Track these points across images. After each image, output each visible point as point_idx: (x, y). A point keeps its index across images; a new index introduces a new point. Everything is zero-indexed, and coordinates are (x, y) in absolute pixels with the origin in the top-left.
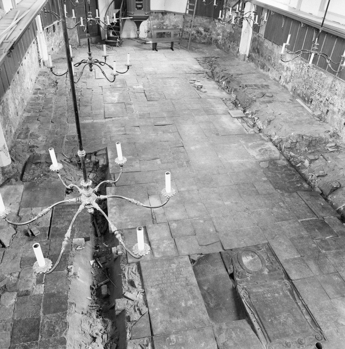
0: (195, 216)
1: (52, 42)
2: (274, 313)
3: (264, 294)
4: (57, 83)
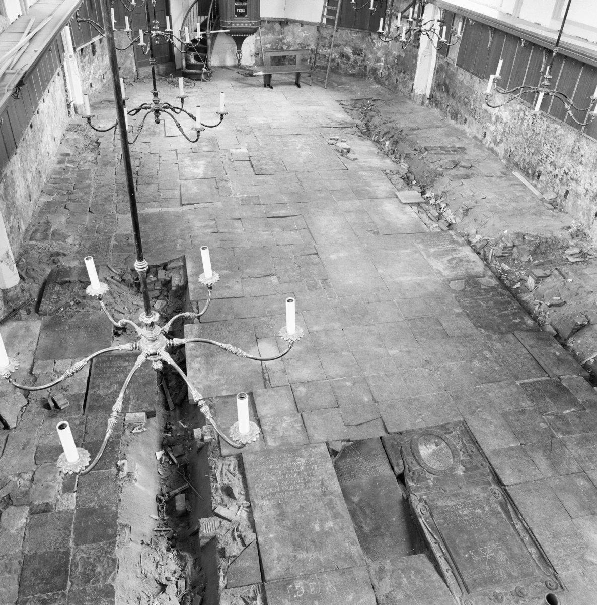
0: (337, 374)
1: (90, 72)
2: (474, 542)
3: (458, 509)
4: (99, 144)
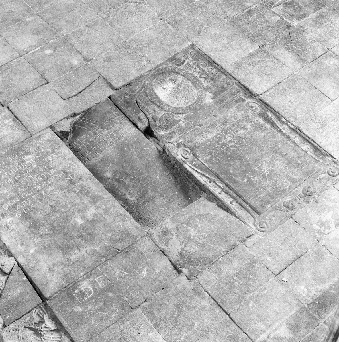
2: (248, 164)
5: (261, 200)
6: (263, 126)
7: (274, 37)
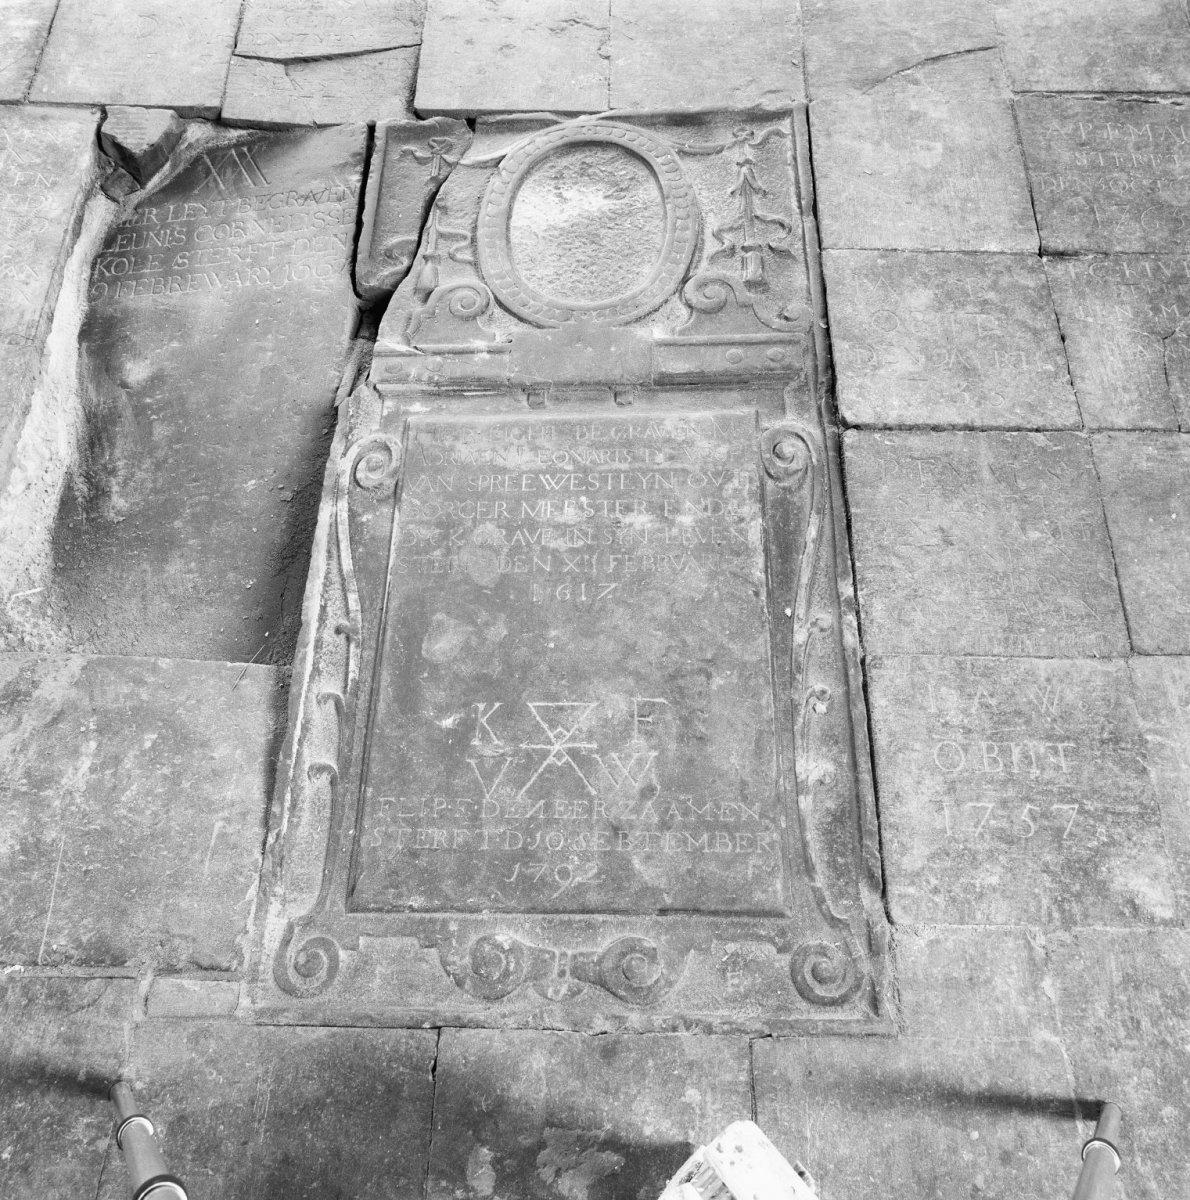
2: (526, 667)
5: (414, 854)
6: (738, 554)
7: (1137, 246)
